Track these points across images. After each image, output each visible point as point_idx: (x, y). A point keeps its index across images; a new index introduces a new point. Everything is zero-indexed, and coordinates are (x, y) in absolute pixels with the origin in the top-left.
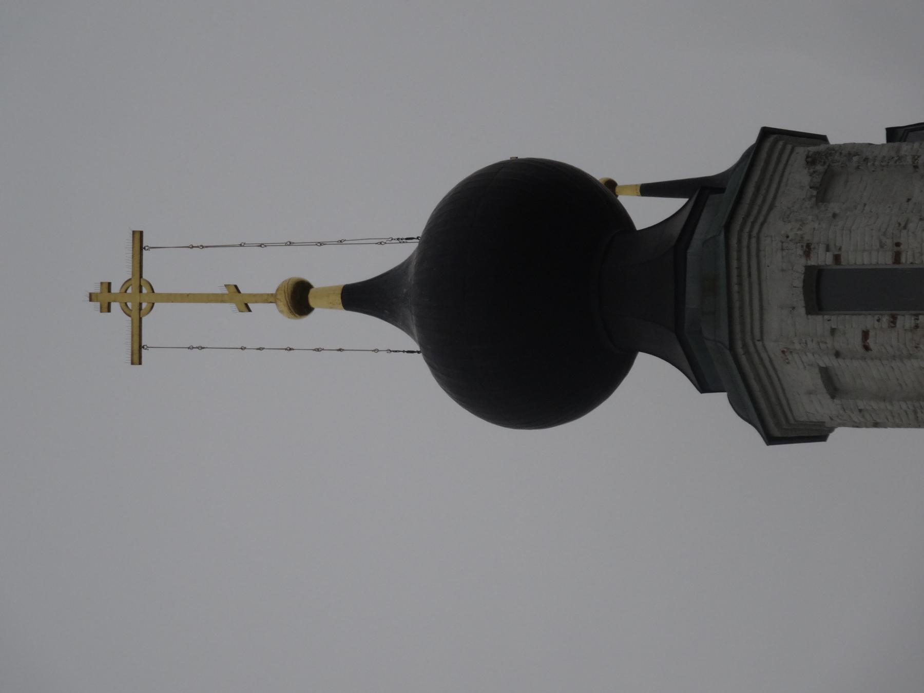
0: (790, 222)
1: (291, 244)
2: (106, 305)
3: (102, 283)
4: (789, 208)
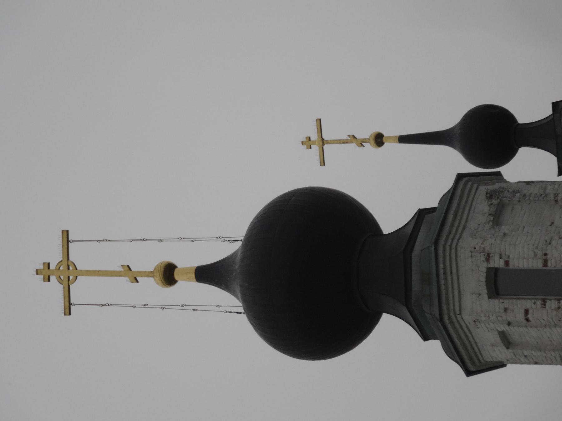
0: (476, 238)
1: (133, 306)
2: (47, 278)
3: (44, 263)
4: (476, 229)
